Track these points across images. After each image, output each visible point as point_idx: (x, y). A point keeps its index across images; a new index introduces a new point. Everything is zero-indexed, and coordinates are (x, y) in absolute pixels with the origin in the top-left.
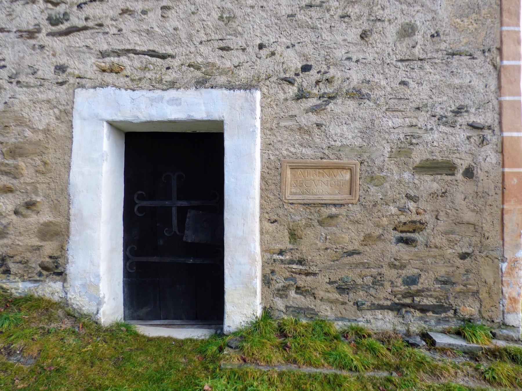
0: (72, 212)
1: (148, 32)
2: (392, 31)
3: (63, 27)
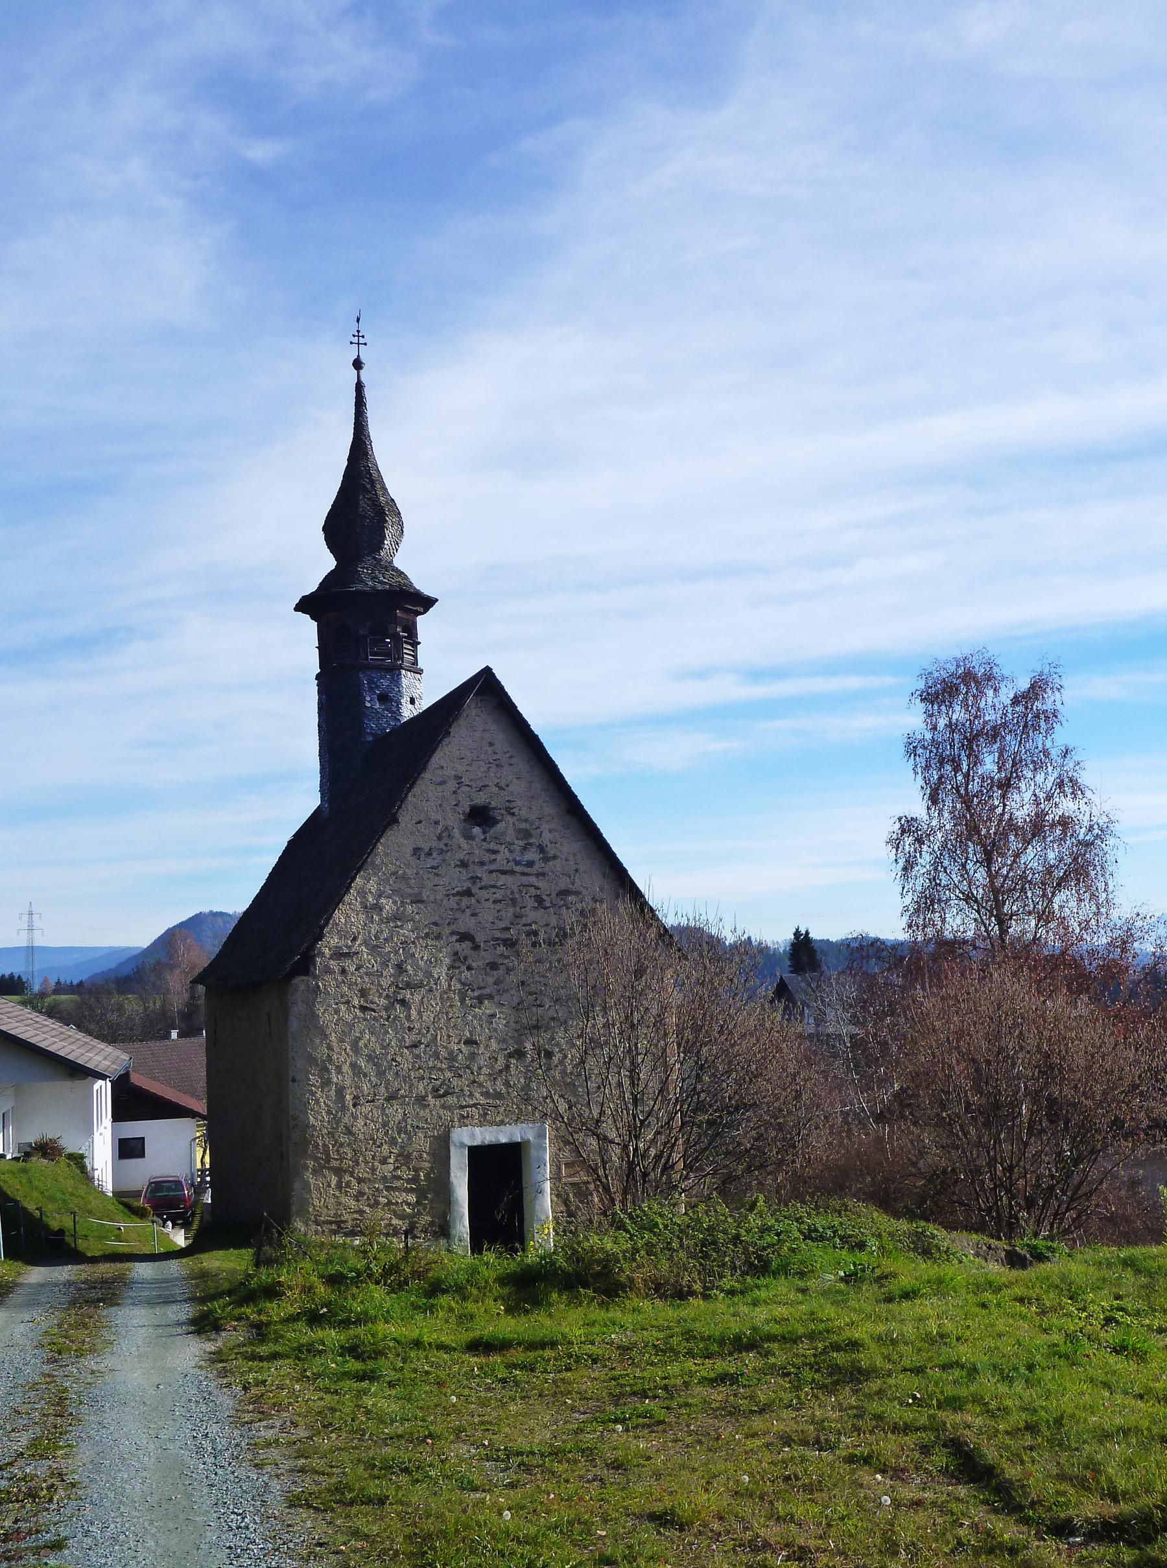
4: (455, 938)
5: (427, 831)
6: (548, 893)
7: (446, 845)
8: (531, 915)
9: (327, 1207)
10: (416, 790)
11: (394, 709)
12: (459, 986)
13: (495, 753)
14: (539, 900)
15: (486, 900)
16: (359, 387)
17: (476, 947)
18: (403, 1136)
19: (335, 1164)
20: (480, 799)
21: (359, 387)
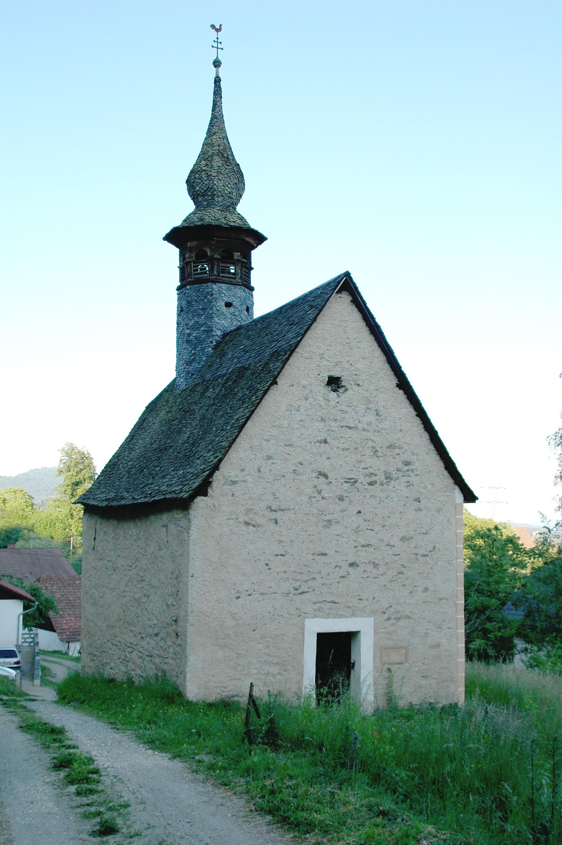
0: (304, 672)
1: (331, 593)
2: (421, 589)
3: (300, 591)
8: (370, 461)
16: (217, 81)
21: (217, 81)
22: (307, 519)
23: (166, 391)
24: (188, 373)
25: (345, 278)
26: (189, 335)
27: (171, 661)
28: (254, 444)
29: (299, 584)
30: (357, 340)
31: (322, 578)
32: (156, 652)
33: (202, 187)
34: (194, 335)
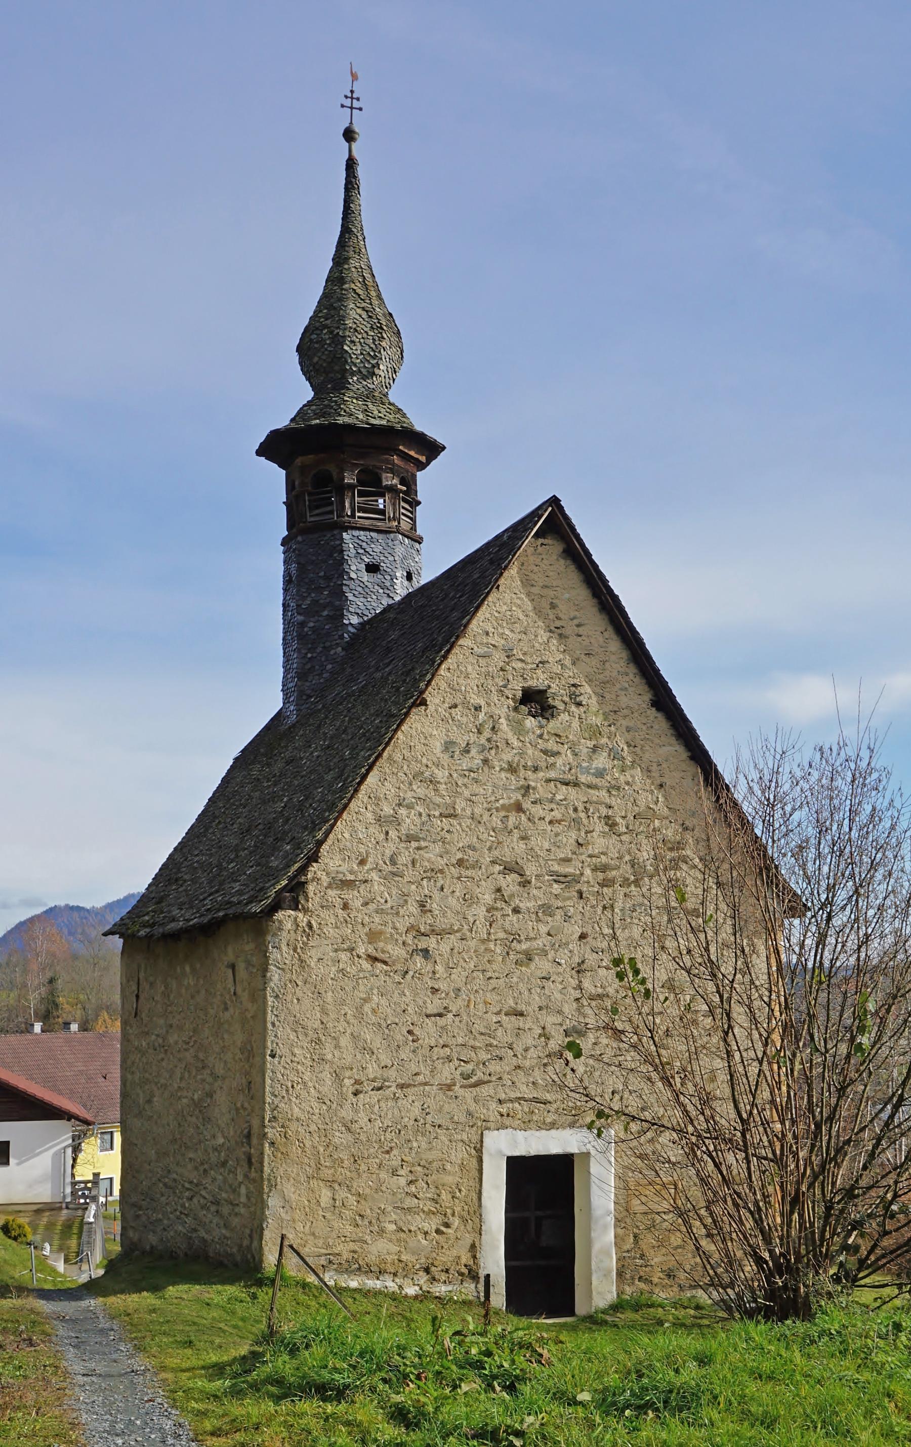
4: (498, 868)
5: (464, 719)
6: (623, 814)
7: (489, 740)
9: (313, 1234)
10: (451, 661)
11: (388, 584)
12: (502, 935)
13: (558, 618)
14: (610, 823)
15: (540, 819)
16: (351, 164)
17: (525, 883)
18: (420, 1138)
19: (327, 1173)
20: (538, 681)
21: (351, 164)
22: (486, 949)
23: (267, 728)
24: (301, 693)
25: (550, 509)
26: (302, 624)
27: (242, 1210)
28: (382, 814)
29: (471, 1068)
30: (576, 622)
31: (515, 1055)
32: (224, 1195)
33: (324, 357)
34: (311, 624)
